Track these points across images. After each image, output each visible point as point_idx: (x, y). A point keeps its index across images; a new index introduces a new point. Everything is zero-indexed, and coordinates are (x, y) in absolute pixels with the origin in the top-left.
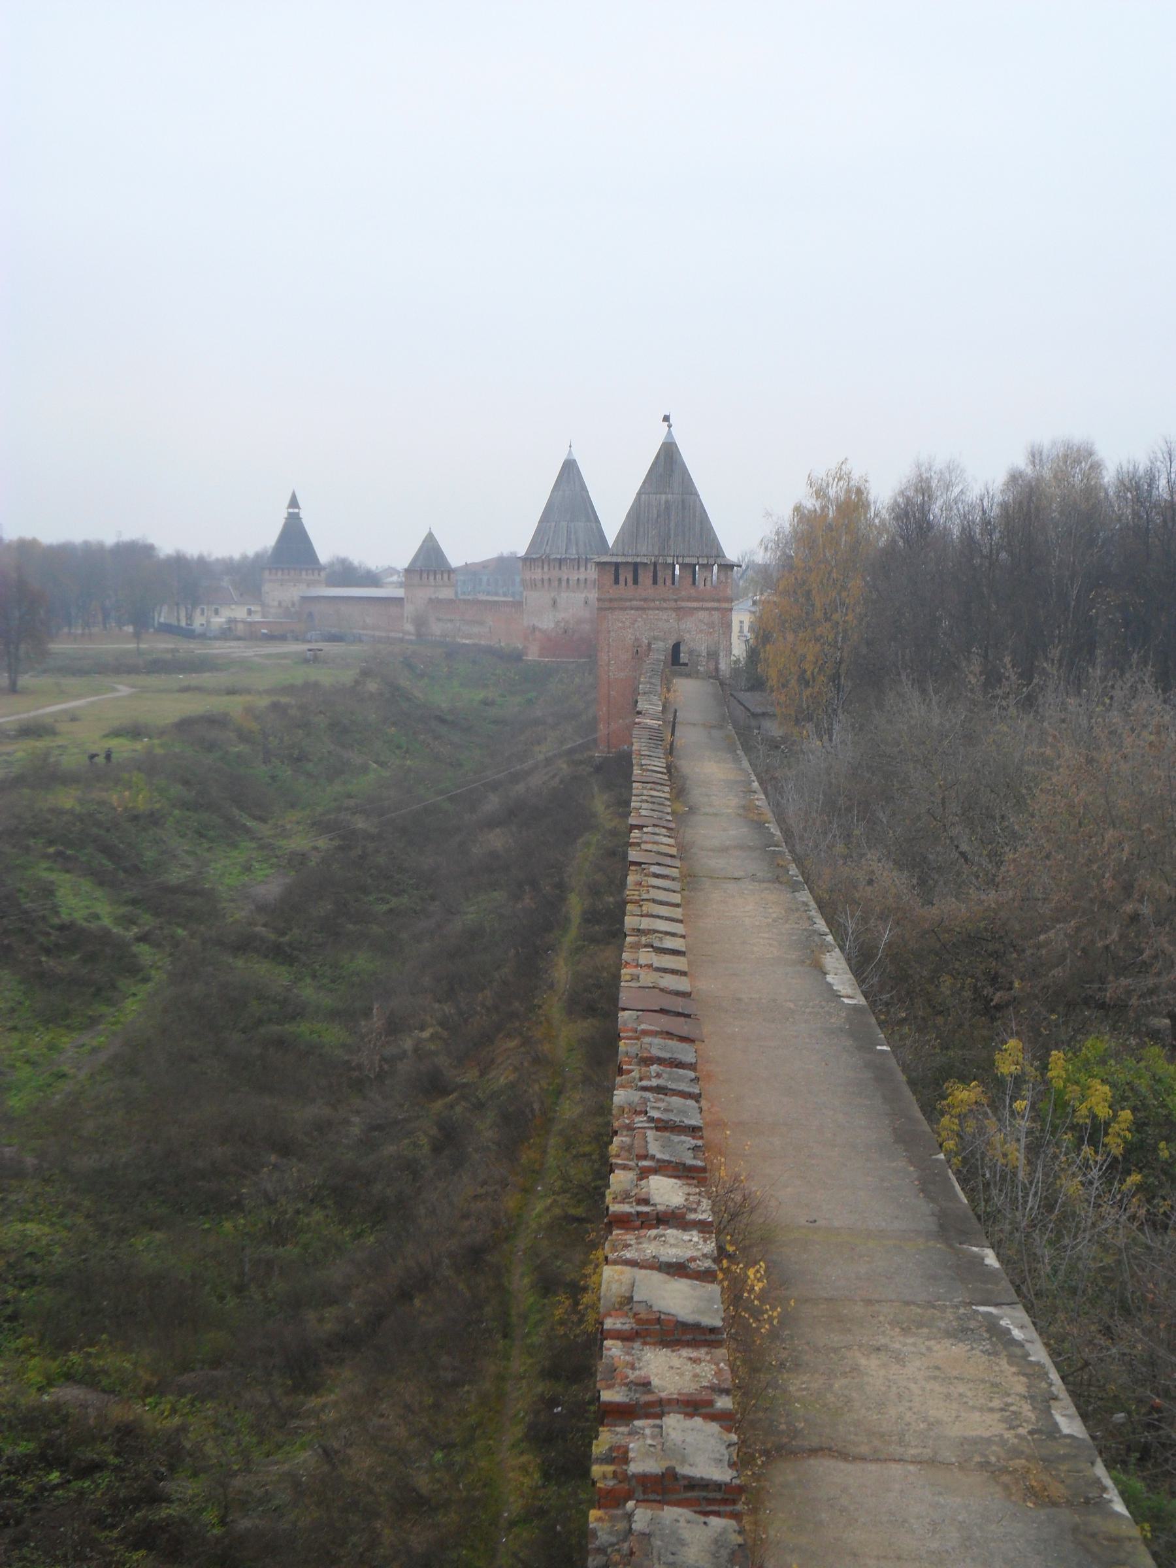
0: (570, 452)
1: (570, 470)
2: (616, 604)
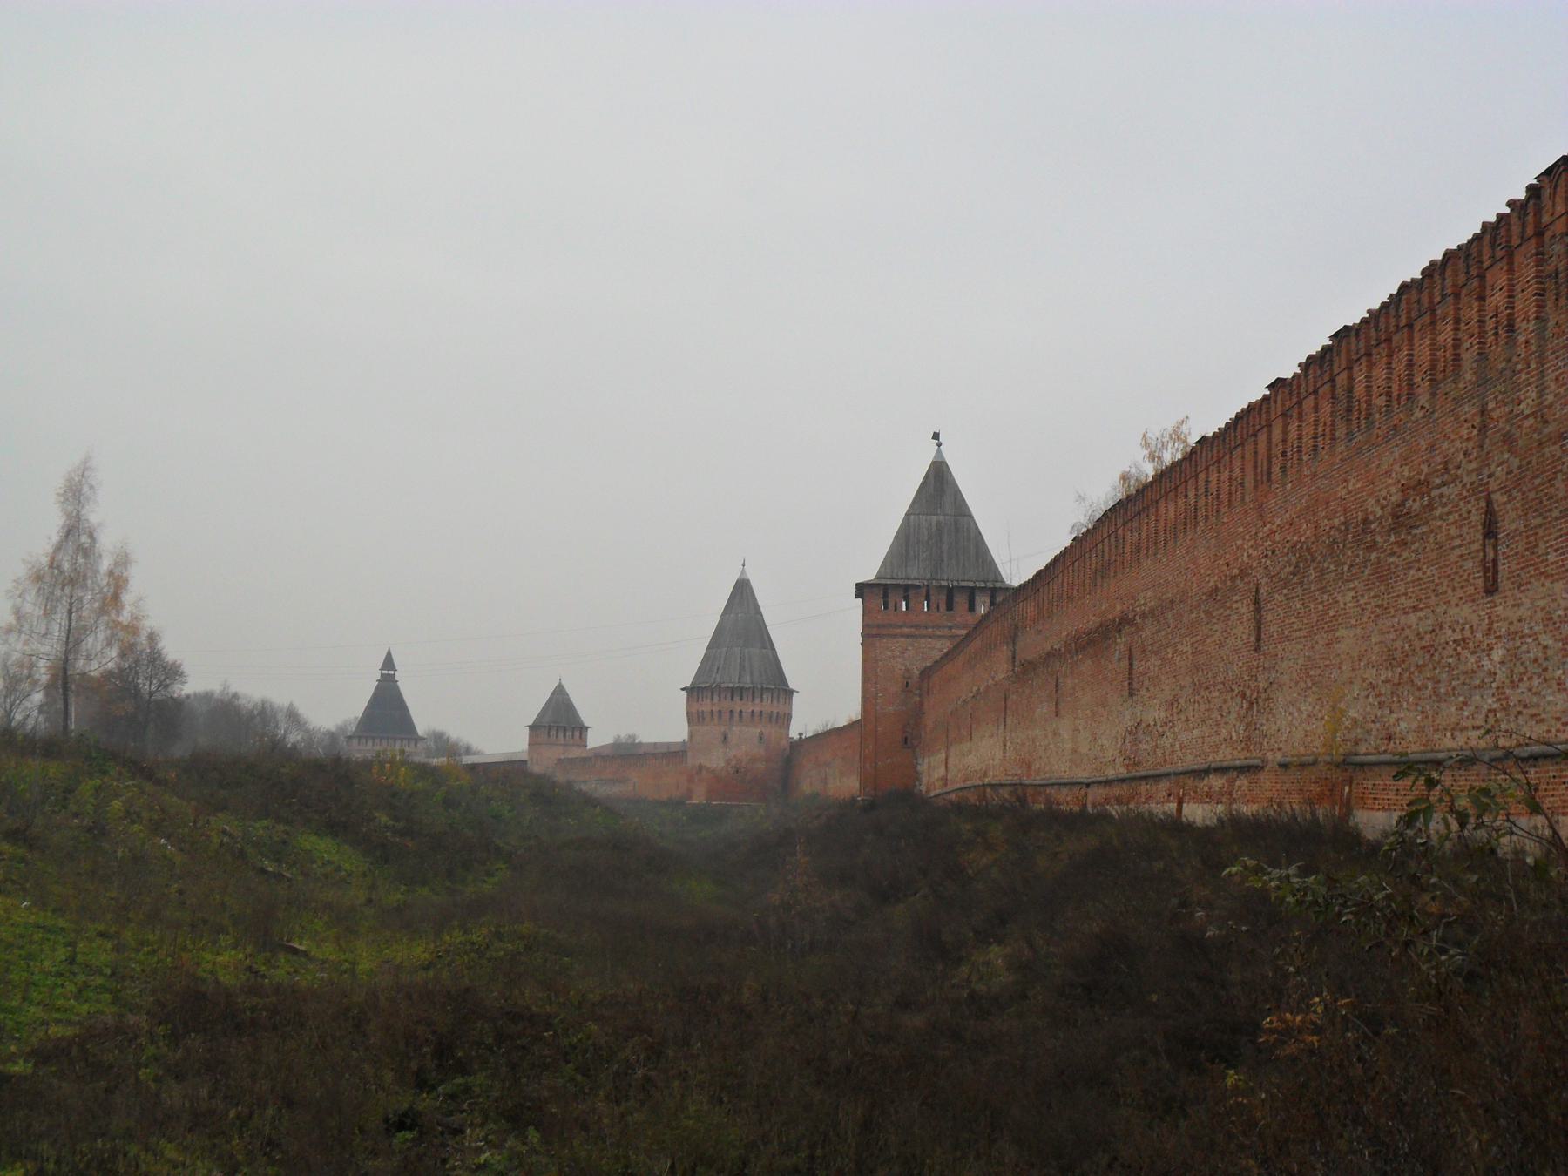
0: (743, 572)
1: (742, 591)
2: (885, 632)
